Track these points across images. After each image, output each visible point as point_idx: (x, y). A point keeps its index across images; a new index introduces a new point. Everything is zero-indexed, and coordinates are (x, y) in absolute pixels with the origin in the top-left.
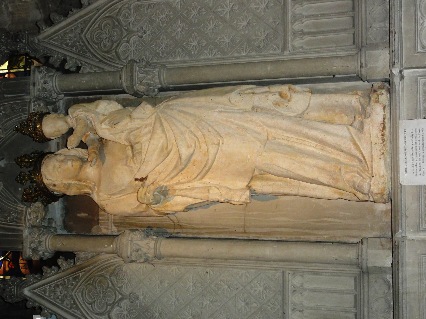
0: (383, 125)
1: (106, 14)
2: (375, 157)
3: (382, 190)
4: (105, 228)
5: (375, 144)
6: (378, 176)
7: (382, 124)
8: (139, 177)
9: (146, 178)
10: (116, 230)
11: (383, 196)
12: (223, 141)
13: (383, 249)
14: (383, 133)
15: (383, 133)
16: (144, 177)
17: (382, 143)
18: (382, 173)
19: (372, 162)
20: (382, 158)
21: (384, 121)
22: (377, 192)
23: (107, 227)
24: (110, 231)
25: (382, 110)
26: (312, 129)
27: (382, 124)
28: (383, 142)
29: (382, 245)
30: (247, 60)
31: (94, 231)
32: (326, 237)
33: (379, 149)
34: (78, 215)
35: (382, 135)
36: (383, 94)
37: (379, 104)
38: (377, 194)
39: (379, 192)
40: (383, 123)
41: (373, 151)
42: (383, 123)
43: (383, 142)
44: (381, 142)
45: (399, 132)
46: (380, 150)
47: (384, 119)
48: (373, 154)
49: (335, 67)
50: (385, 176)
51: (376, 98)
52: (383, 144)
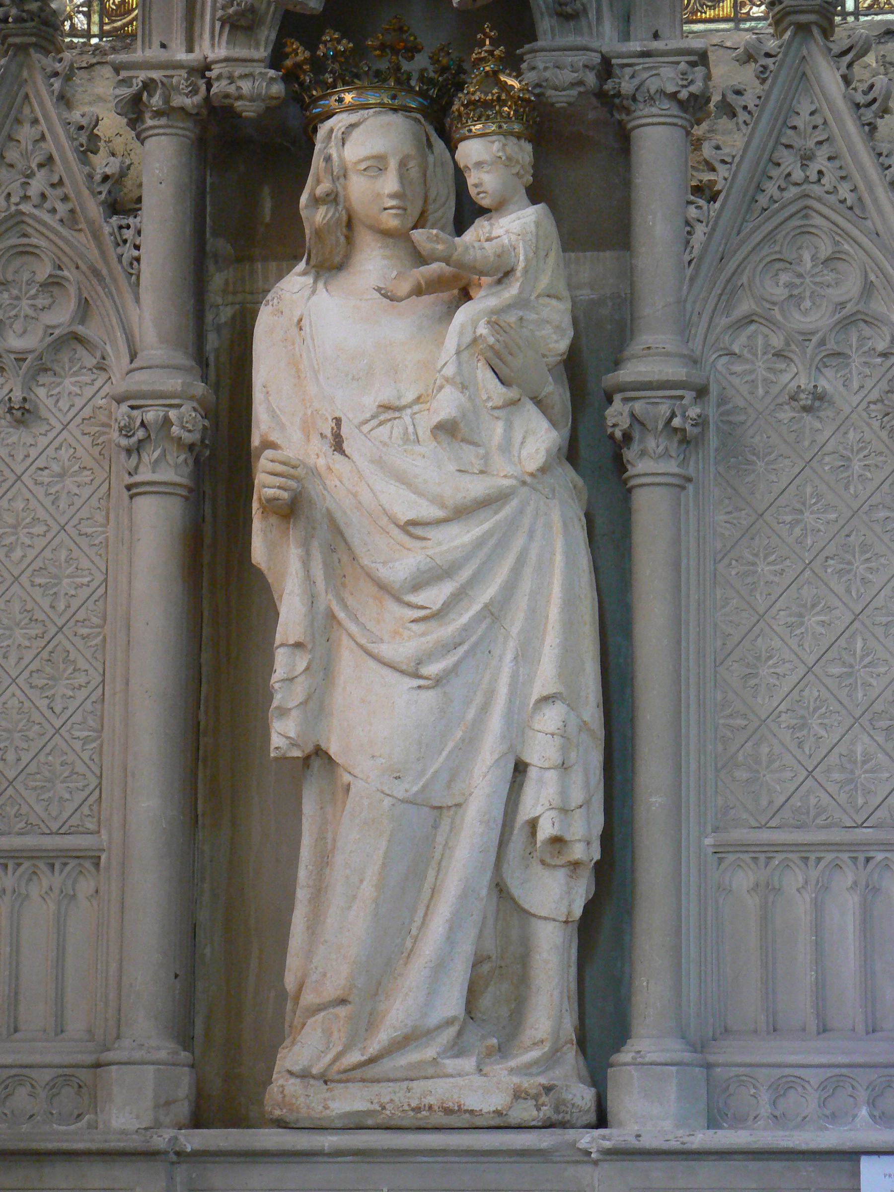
0: (456, 1108)
1: (873, 271)
2: (376, 1088)
3: (293, 1105)
4: (227, 283)
5: (409, 1090)
6: (328, 1095)
7: (459, 1106)
8: (344, 432)
9: (342, 452)
10: (223, 319)
11: (279, 1106)
12: (428, 688)
13: (157, 1106)
14: (436, 1108)
15: (436, 1108)
16: (345, 446)
17: (409, 1105)
18: (331, 1104)
19: (363, 1080)
20: (371, 1107)
21: (466, 1111)
22: (286, 1092)
23: (231, 288)
24: (219, 300)
25: (493, 1108)
26: (451, 929)
27: (459, 1106)
28: (413, 1110)
29: (167, 1104)
30: (693, 731)
31: (218, 245)
32: (208, 951)
33: (396, 1100)
34: (266, 190)
35: (430, 1107)
36: (538, 1110)
37: (509, 1099)
38: (282, 1092)
39: (287, 1099)
40: (459, 1110)
41: (391, 1084)
42: (459, 1110)
43: (413, 1110)
44: (413, 1105)
45: (664, 1160)
46: (392, 1100)
47: (472, 1112)
48: (382, 1084)
49: (645, 984)
50: (328, 1112)
51: (527, 1093)
52: (406, 1108)
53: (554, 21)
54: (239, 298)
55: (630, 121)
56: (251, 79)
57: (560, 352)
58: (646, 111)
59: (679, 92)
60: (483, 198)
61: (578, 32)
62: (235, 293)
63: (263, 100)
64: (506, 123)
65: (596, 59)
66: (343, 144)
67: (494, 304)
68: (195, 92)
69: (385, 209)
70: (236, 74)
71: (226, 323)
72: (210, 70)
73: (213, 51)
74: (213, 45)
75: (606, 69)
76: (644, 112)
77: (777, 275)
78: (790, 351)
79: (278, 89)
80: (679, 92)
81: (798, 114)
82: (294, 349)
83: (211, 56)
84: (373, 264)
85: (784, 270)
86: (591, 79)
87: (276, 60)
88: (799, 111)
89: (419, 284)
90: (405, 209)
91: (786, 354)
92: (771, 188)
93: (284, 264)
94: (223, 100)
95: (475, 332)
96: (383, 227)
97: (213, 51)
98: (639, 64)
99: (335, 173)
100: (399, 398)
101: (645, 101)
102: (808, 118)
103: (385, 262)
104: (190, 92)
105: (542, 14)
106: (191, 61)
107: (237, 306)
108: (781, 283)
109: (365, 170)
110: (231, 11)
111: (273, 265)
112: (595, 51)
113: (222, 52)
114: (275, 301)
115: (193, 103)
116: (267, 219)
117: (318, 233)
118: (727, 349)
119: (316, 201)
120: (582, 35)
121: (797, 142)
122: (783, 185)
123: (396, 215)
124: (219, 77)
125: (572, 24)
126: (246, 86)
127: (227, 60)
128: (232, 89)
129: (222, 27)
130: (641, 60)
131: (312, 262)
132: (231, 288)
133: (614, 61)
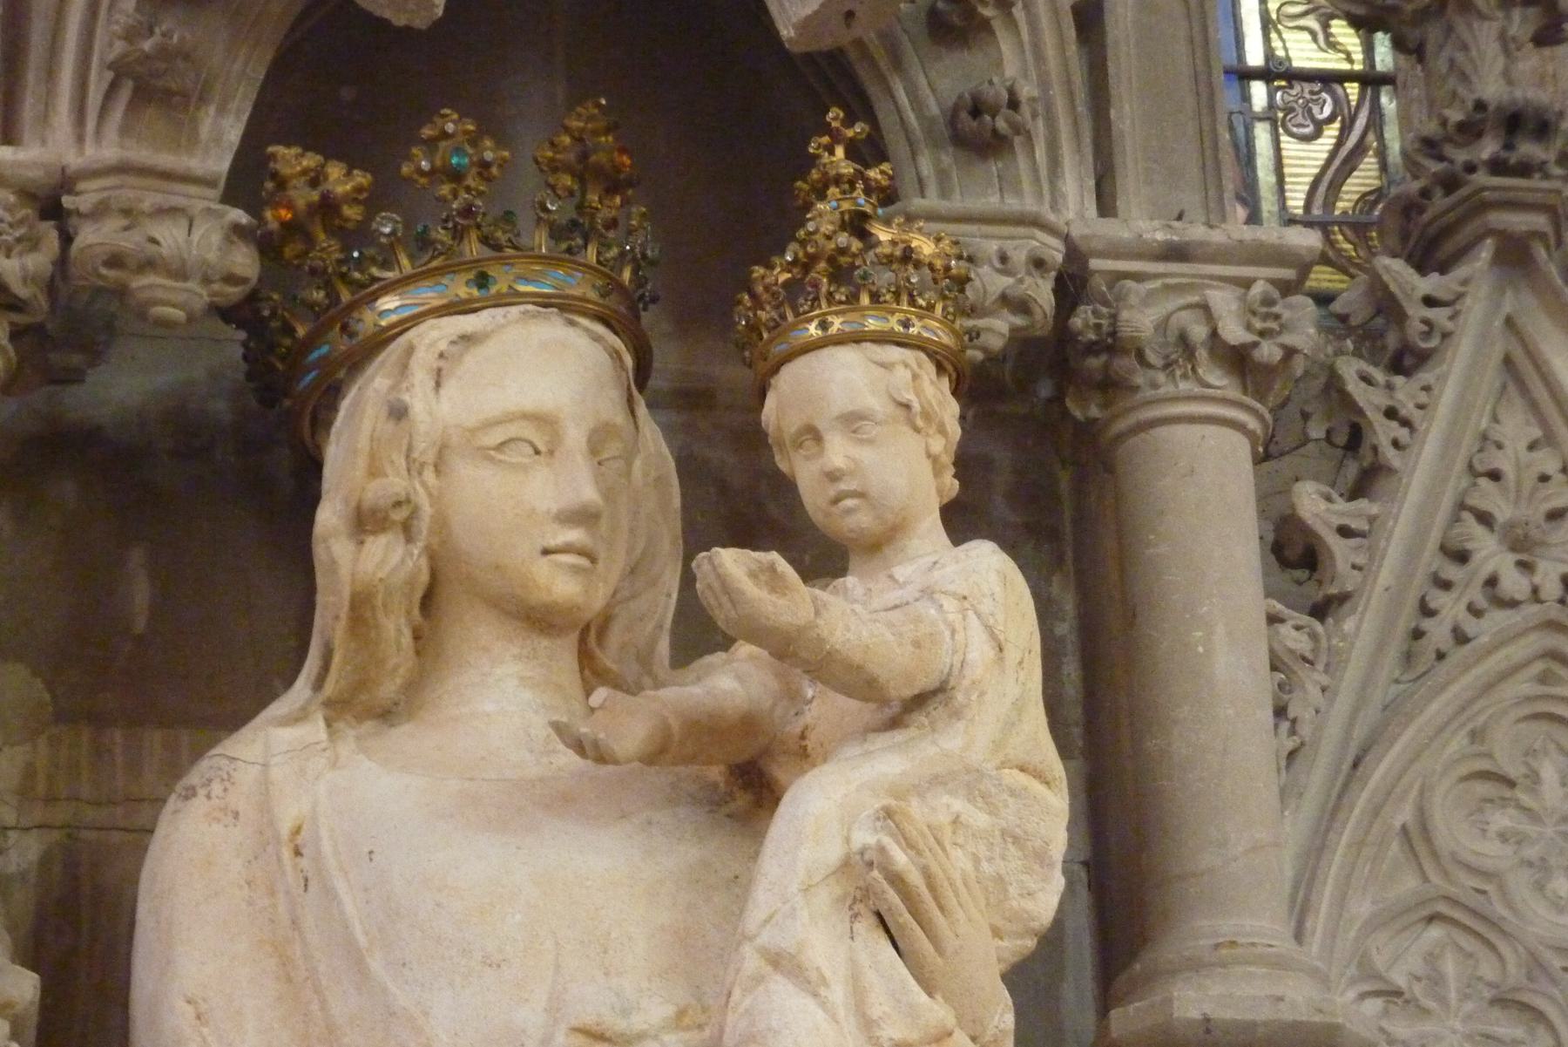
4: (29, 773)
53: (947, 159)
54: (62, 813)
55: (1115, 417)
56: (184, 223)
57: (1035, 925)
58: (1167, 389)
59: (1255, 345)
60: (849, 511)
61: (1008, 184)
62: (51, 799)
63: (207, 281)
64: (921, 318)
65: (1055, 252)
66: (438, 385)
67: (898, 770)
68: (33, 243)
69: (546, 552)
70: (146, 206)
71: (23, 876)
72: (71, 192)
73: (81, 151)
74: (80, 139)
75: (1072, 284)
76: (1164, 392)
77: (1481, 810)
78: (1535, 991)
79: (245, 261)
80: (1255, 345)
81: (1499, 446)
82: (274, 906)
83: (73, 160)
84: (504, 700)
85: (1504, 802)
86: (1043, 293)
87: (248, 180)
88: (1501, 439)
89: (666, 730)
90: (593, 559)
91: (1525, 998)
92: (1451, 607)
93: (185, 737)
94: (104, 271)
95: (848, 840)
96: (538, 597)
97: (81, 151)
98: (1156, 276)
99: (415, 455)
100: (625, 1013)
101: (1167, 366)
102: (1525, 456)
103: (527, 695)
104: (19, 240)
105: (911, 144)
106: (20, 164)
107: (56, 835)
108: (1493, 828)
109: (500, 447)
110: (147, 45)
111: (154, 739)
112: (1051, 230)
113: (109, 151)
114: (217, 788)
115: (23, 268)
116: (140, 625)
117: (361, 608)
118: (1378, 977)
119: (365, 522)
120: (1018, 192)
121: (1503, 512)
122: (1481, 602)
123: (576, 570)
124: (99, 212)
125: (994, 167)
126: (170, 237)
127: (122, 169)
128: (130, 242)
129: (113, 87)
130: (1160, 267)
131: (329, 688)
132: (41, 788)
133: (1095, 264)
